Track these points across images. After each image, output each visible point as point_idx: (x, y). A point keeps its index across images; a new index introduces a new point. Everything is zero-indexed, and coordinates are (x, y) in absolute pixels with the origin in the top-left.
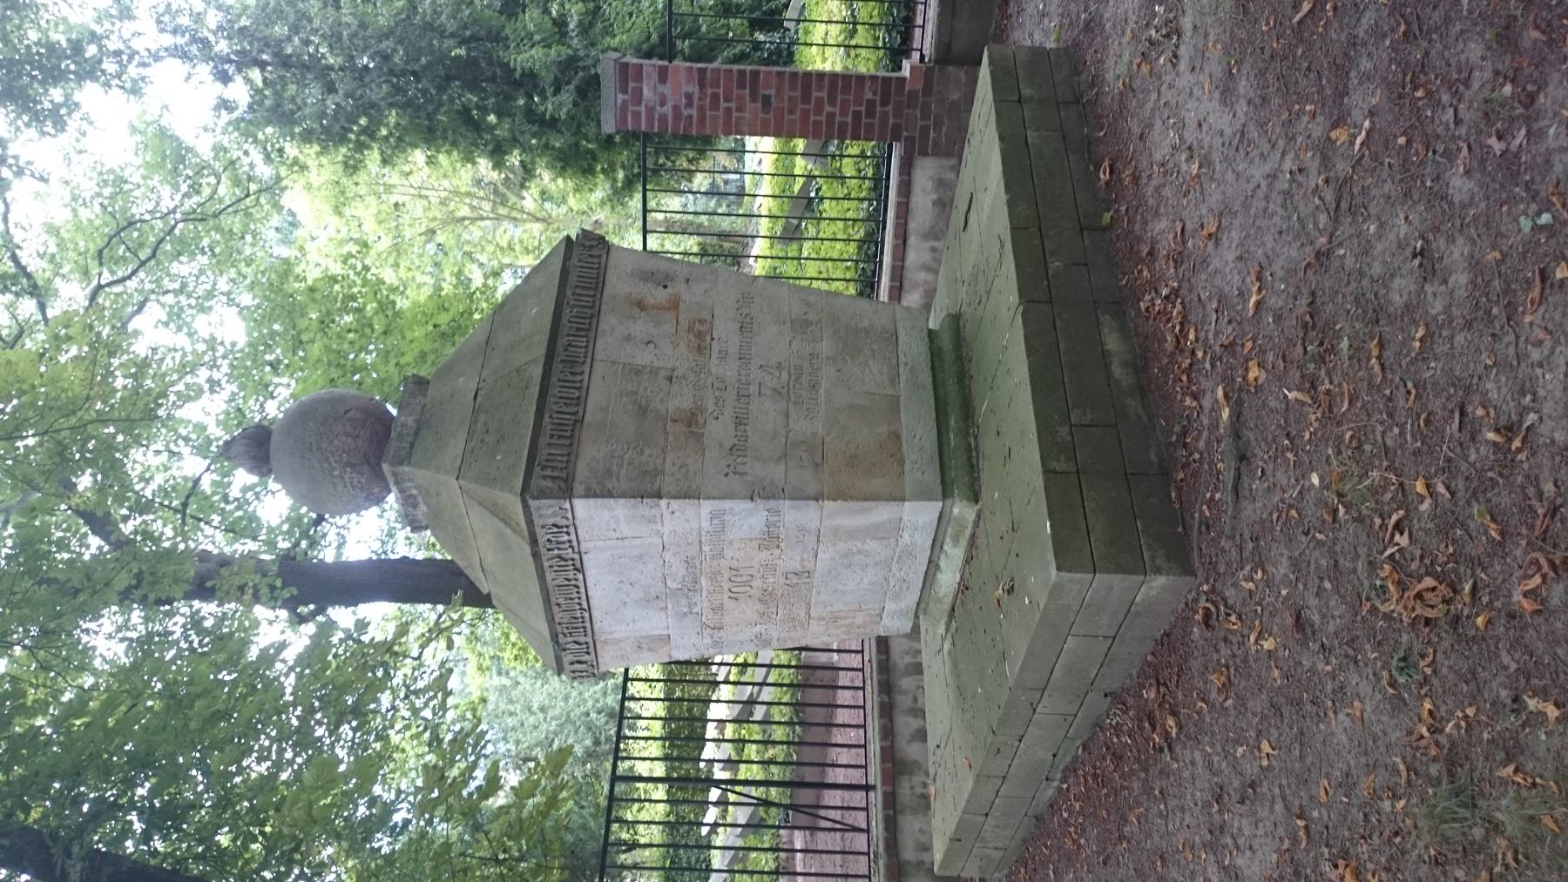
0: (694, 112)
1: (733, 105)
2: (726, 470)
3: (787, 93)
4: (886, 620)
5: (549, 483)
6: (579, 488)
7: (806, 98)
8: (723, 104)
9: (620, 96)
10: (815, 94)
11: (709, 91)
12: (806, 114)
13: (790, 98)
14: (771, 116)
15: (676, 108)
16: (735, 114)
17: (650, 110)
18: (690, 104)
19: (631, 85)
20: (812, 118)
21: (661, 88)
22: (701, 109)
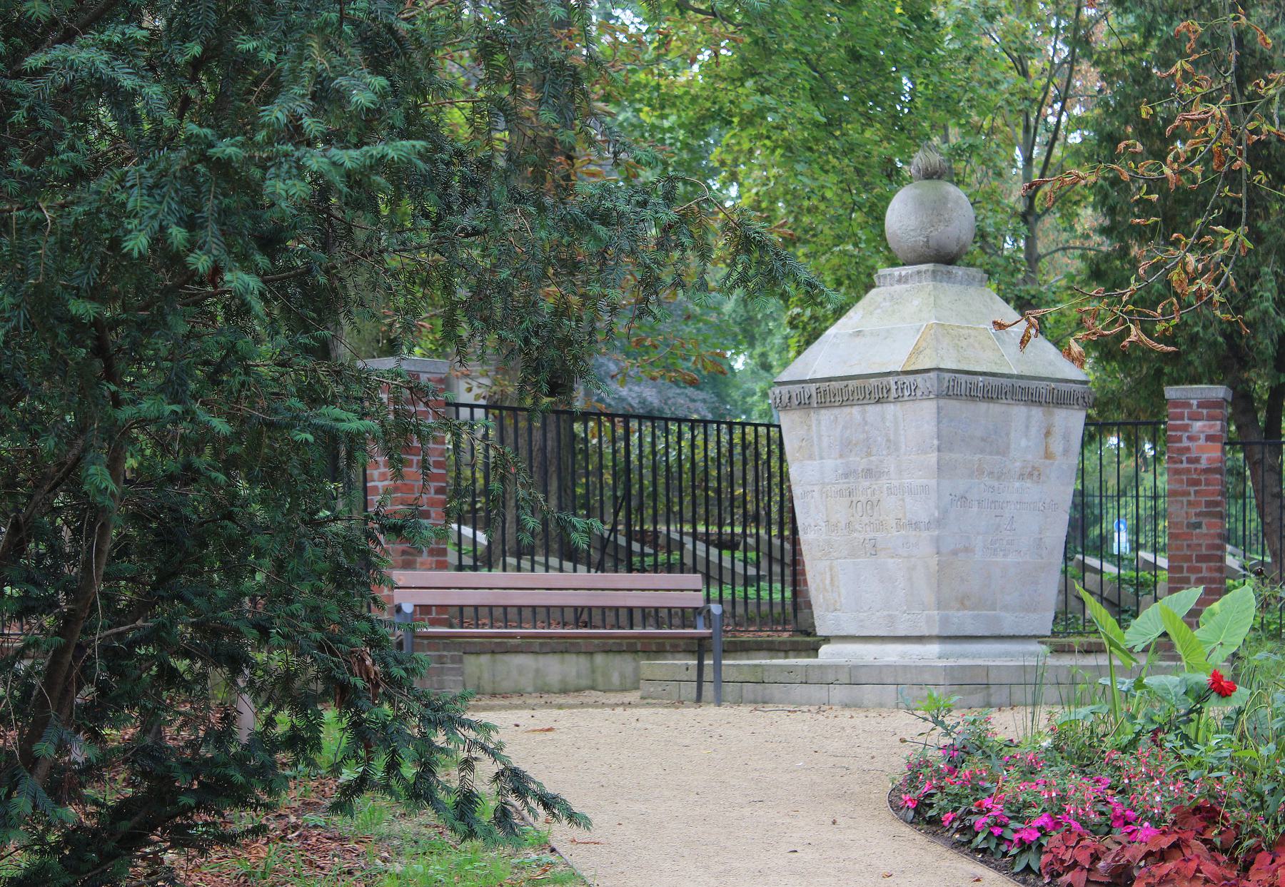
0: (1185, 465)
1: (1192, 498)
3: (1204, 542)
4: (830, 615)
5: (946, 385)
6: (942, 402)
7: (1201, 558)
8: (1192, 489)
9: (1195, 402)
10: (1204, 565)
11: (1203, 478)
12: (1188, 559)
13: (1200, 545)
14: (1185, 530)
15: (1188, 449)
16: (1185, 499)
17: (1185, 428)
18: (1190, 461)
19: (1205, 411)
20: (1185, 565)
21: (1202, 436)
22: (1188, 471)
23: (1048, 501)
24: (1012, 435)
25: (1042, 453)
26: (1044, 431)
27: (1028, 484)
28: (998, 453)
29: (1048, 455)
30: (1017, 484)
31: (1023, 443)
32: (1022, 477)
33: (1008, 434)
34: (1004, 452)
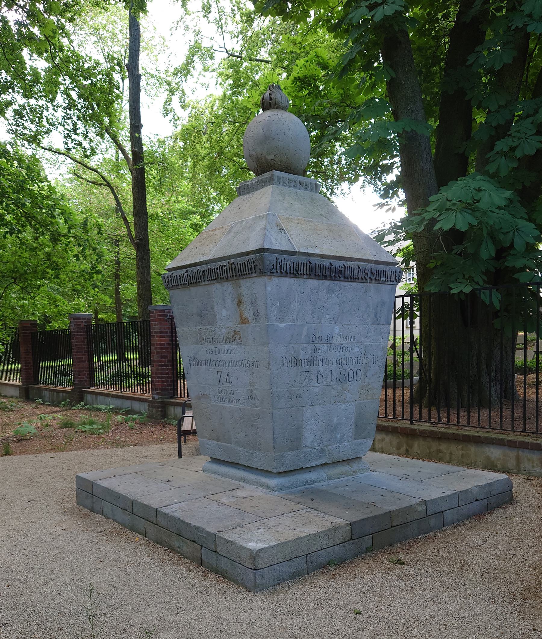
2: (190, 356)
23: (251, 359)
24: (216, 308)
25: (239, 319)
26: (236, 301)
27: (234, 346)
28: (209, 324)
29: (244, 321)
30: (227, 347)
31: (224, 313)
32: (228, 340)
33: (212, 308)
34: (212, 322)
